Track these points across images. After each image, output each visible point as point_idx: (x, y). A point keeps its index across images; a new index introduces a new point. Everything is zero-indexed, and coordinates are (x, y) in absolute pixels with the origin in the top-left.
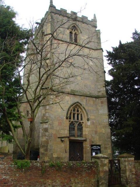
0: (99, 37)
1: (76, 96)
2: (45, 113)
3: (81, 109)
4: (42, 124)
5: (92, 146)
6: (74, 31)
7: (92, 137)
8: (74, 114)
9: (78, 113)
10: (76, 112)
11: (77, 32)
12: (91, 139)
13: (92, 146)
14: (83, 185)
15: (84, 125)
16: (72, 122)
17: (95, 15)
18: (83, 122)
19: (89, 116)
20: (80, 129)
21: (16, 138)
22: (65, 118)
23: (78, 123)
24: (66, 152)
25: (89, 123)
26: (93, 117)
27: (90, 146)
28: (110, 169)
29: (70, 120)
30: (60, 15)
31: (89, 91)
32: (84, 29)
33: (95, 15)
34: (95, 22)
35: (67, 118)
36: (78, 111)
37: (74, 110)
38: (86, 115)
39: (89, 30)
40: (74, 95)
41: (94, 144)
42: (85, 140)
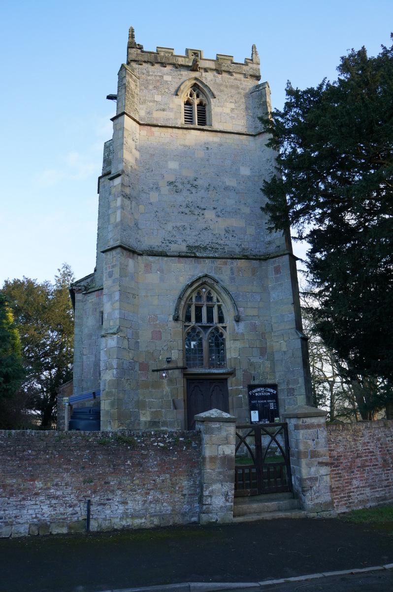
0: (263, 100)
1: (202, 260)
2: (111, 310)
3: (218, 293)
4: (104, 339)
5: (251, 387)
6: (198, 96)
7: (251, 364)
8: (199, 309)
9: (210, 303)
10: (204, 302)
11: (204, 99)
12: (248, 368)
13: (251, 387)
14: (150, 497)
15: (227, 335)
16: (193, 329)
17: (254, 47)
18: (225, 328)
19: (241, 309)
20: (218, 342)
21: (271, 381)
22: (171, 318)
23: (187, 329)
24: (175, 408)
25: (241, 328)
26: (254, 312)
27: (246, 389)
28: (254, 453)
29: (187, 324)
30: (153, 65)
31: (239, 243)
32: (222, 88)
33: (254, 47)
34: (255, 66)
35: (176, 319)
36: (210, 298)
37: (199, 297)
38: (181, 307)
39: (238, 88)
40: (196, 257)
41: (256, 382)
42: (232, 373)
